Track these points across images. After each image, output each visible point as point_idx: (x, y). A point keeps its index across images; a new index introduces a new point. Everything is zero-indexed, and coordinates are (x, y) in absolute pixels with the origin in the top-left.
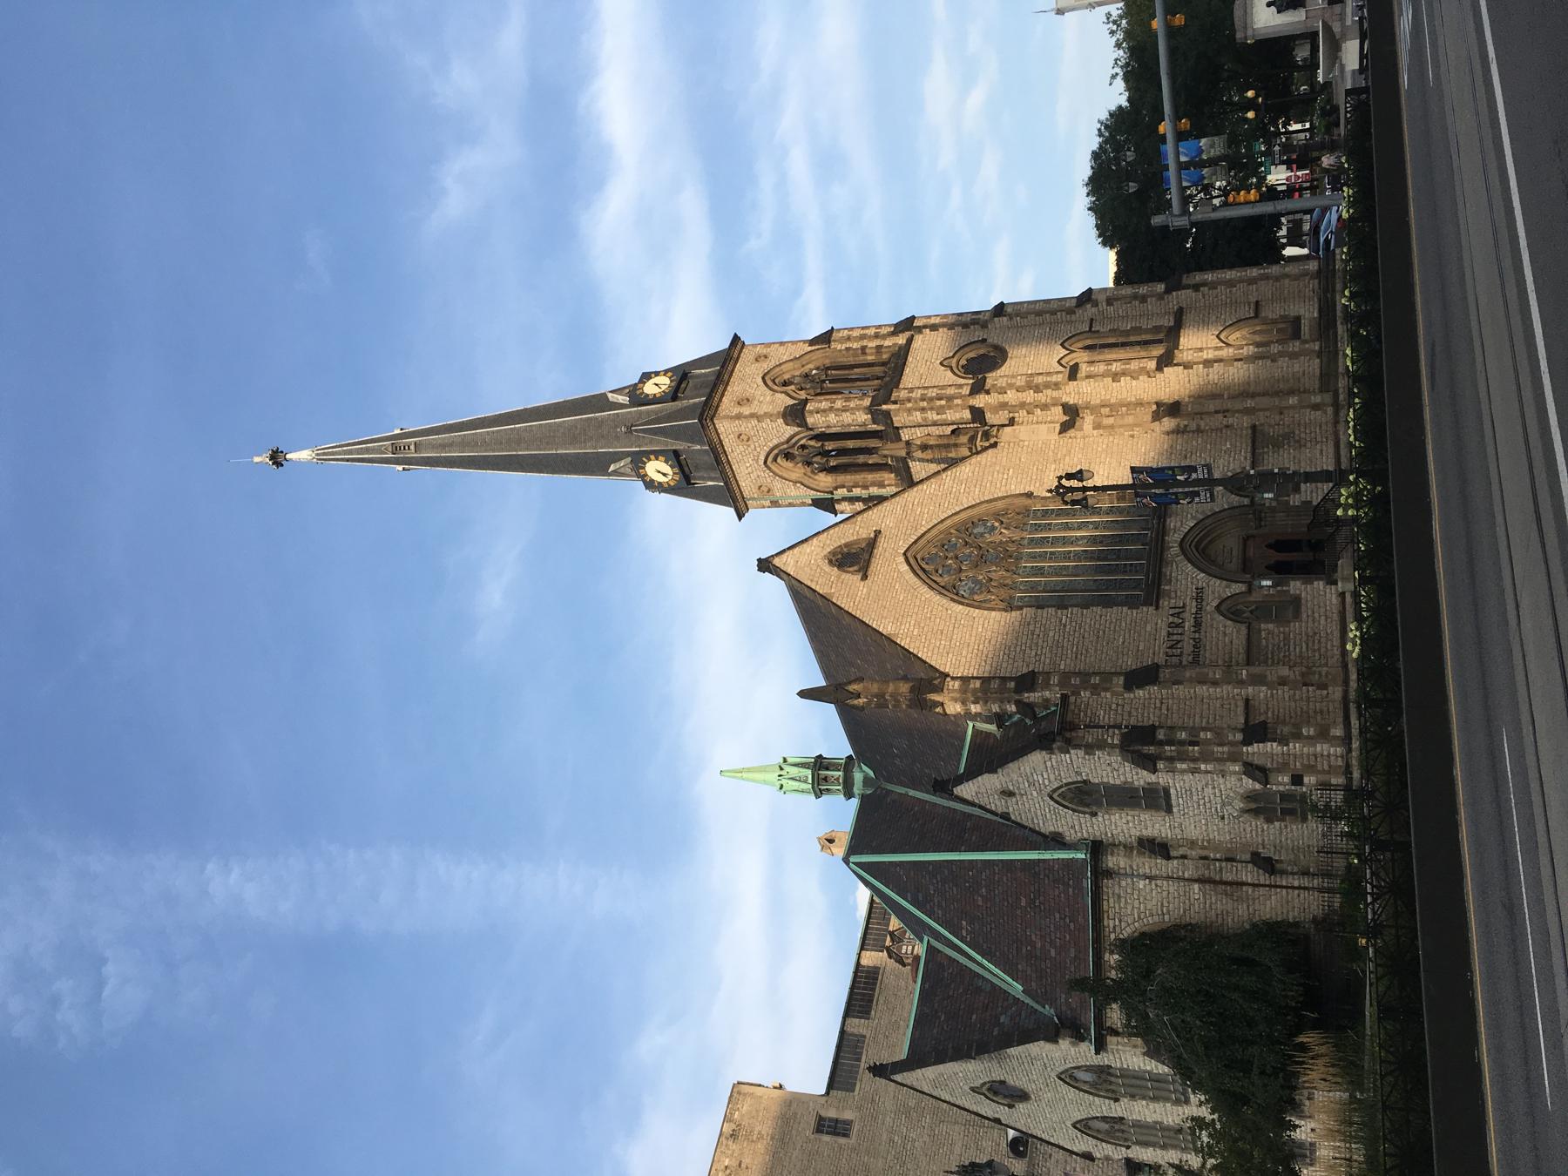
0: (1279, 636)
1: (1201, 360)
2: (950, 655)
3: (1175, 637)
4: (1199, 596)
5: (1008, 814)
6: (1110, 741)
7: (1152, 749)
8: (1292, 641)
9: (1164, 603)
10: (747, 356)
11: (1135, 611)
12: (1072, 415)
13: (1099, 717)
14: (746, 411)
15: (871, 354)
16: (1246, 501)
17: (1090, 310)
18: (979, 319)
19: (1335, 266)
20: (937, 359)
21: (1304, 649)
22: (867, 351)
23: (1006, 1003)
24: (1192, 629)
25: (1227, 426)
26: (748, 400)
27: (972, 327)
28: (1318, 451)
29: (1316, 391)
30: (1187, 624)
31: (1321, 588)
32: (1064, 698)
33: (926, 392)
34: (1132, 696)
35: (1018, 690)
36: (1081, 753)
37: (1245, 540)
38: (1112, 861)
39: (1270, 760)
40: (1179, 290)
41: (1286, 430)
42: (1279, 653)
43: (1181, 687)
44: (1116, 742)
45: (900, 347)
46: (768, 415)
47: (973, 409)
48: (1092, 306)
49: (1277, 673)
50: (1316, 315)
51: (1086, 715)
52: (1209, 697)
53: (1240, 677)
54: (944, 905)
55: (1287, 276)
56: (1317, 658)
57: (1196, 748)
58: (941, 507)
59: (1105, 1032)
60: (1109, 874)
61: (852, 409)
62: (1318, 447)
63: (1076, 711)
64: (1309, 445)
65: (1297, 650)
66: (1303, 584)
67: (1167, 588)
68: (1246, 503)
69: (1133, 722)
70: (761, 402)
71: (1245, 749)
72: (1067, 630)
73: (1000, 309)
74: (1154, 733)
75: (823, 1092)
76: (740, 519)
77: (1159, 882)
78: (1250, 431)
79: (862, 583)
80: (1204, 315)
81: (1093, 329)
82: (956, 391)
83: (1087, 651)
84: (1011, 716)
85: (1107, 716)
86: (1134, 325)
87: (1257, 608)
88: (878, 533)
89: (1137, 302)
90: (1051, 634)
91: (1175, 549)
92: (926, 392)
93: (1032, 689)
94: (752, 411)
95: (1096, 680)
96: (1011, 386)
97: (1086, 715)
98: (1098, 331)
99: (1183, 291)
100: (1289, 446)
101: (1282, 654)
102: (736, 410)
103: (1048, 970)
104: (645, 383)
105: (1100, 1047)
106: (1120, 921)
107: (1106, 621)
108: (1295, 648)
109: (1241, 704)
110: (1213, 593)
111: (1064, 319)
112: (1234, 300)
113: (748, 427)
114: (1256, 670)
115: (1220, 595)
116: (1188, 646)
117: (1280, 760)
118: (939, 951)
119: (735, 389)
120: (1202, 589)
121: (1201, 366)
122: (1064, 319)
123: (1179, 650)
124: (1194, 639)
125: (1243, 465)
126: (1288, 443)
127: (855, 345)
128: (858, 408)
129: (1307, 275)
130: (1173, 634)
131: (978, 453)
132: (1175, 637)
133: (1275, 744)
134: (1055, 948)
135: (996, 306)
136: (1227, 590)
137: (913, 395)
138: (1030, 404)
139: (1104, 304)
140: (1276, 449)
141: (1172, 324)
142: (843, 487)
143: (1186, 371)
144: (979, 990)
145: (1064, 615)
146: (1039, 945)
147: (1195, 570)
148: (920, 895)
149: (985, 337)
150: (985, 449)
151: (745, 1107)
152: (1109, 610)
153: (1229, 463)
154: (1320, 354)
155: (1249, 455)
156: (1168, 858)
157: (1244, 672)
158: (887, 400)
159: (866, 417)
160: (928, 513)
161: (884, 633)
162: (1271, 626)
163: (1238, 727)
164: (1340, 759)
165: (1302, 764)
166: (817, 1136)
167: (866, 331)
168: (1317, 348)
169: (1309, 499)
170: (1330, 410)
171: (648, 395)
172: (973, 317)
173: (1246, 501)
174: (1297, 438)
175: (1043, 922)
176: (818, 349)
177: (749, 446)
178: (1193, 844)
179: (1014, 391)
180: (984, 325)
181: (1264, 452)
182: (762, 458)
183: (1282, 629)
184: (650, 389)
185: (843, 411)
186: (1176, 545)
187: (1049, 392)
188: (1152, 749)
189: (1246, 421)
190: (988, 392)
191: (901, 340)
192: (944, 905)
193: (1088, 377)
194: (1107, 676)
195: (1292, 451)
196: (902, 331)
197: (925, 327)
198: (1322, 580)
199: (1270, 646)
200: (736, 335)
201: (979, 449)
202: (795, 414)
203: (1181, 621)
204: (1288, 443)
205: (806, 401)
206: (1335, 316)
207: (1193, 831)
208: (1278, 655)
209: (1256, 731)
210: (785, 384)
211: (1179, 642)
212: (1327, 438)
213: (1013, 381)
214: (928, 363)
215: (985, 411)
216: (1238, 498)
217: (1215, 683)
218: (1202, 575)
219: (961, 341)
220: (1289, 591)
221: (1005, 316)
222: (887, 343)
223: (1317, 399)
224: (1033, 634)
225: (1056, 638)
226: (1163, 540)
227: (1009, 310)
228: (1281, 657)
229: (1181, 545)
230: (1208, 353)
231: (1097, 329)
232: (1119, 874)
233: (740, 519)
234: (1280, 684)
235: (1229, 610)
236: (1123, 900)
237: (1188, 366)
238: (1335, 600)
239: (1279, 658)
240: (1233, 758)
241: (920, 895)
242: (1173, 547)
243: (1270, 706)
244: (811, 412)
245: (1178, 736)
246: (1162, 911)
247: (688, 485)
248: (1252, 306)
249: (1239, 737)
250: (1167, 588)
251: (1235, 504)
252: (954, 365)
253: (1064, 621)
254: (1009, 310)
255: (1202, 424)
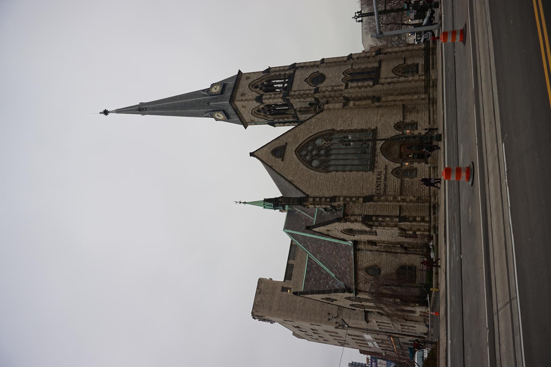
0: (410, 183)
1: (387, 82)
2: (309, 188)
3: (378, 183)
4: (386, 168)
5: (329, 234)
6: (358, 220)
7: (371, 223)
8: (414, 184)
9: (375, 170)
10: (244, 78)
11: (366, 173)
12: (347, 100)
13: (355, 211)
14: (244, 98)
15: (282, 76)
16: (401, 133)
17: (351, 61)
18: (316, 64)
19: (430, 47)
20: (303, 79)
21: (418, 187)
22: (281, 75)
23: (330, 279)
24: (384, 180)
25: (395, 105)
26: (244, 94)
27: (314, 67)
28: (423, 114)
29: (423, 93)
30: (382, 179)
31: (424, 165)
32: (345, 205)
33: (300, 92)
34: (365, 204)
35: (331, 201)
36: (350, 223)
37: (401, 146)
38: (361, 246)
39: (406, 227)
40: (380, 54)
41: (414, 106)
42: (410, 189)
43: (380, 202)
44: (360, 220)
45: (292, 74)
46: (250, 100)
47: (315, 98)
48: (352, 60)
49: (409, 198)
50: (423, 63)
51: (351, 211)
52: (389, 205)
53: (398, 199)
54: (312, 248)
55: (414, 50)
56: (422, 190)
57: (384, 223)
58: (306, 134)
59: (358, 291)
60: (359, 250)
61: (277, 98)
62: (424, 112)
63: (348, 209)
64: (420, 111)
65: (416, 188)
66: (418, 163)
67: (376, 165)
68: (401, 134)
69: (365, 213)
70: (249, 95)
71: (399, 223)
72: (345, 179)
73: (323, 60)
74: (373, 197)
75: (283, 280)
76: (246, 129)
77: (373, 252)
78: (402, 106)
79: (282, 162)
80: (388, 63)
81: (353, 68)
82: (309, 92)
83: (351, 188)
84: (328, 208)
85: (357, 211)
86: (365, 66)
87: (404, 172)
88: (286, 143)
89: (367, 59)
90: (341, 181)
91: (379, 150)
92: (300, 92)
93: (335, 202)
94: (246, 98)
95: (354, 199)
96: (327, 90)
97: (351, 211)
98: (354, 68)
99: (381, 55)
100: (415, 112)
101: (411, 189)
102: (241, 98)
103: (342, 272)
104: (212, 88)
105: (356, 294)
106: (362, 262)
107: (357, 176)
108: (415, 187)
109: (398, 207)
110: (390, 167)
111: (343, 64)
112: (397, 57)
113: (245, 103)
114: (403, 197)
115: (392, 168)
116: (382, 186)
117: (410, 227)
118: (311, 259)
119: (240, 90)
120: (387, 165)
121: (387, 84)
122: (343, 64)
123: (380, 188)
124: (384, 183)
125: (400, 119)
126: (414, 111)
127: (277, 73)
128: (279, 98)
129: (421, 49)
130: (378, 182)
131: (317, 114)
132: (378, 183)
133: (408, 223)
134: (344, 267)
135: (321, 59)
136: (395, 166)
137: (296, 93)
138: (333, 96)
139: (356, 59)
140: (410, 113)
141: (378, 66)
142: (276, 119)
143: (382, 86)
144: (322, 273)
145: (344, 174)
146: (339, 265)
147: (385, 158)
148: (305, 245)
149: (318, 70)
150: (319, 112)
151: (262, 285)
152: (358, 173)
153: (396, 118)
154: (424, 80)
155: (402, 116)
156: (376, 246)
157: (399, 198)
158: (288, 95)
159: (281, 100)
160: (302, 136)
161: (289, 180)
162: (408, 179)
163: (397, 215)
164: (427, 226)
165: (416, 229)
166: (282, 292)
167: (280, 68)
168: (424, 78)
169: (420, 132)
170: (427, 100)
171: (213, 93)
172: (314, 63)
173: (401, 133)
174: (417, 109)
175: (340, 260)
176: (266, 75)
177: (246, 109)
178: (383, 242)
179: (328, 92)
180: (318, 66)
181: (406, 114)
182: (250, 111)
183: (411, 180)
184: (213, 90)
185: (274, 99)
186: (379, 149)
187: (339, 92)
188: (371, 223)
189: (401, 103)
190: (319, 93)
191: (292, 72)
192: (312, 248)
193: (351, 88)
194: (358, 198)
195: (415, 114)
196: (292, 68)
197: (299, 67)
198: (424, 162)
199: (407, 187)
200: (239, 70)
201: (318, 112)
202: (259, 99)
203: (380, 177)
204: (414, 111)
205: (262, 95)
206: (430, 64)
207: (383, 239)
208: (410, 189)
209: (403, 219)
210: (257, 87)
211: (380, 184)
212: (426, 109)
213: (327, 89)
214: (300, 80)
215: (319, 99)
216: (398, 131)
217: (390, 202)
218: (387, 160)
219: (311, 72)
220: (413, 166)
221: (324, 63)
222: (287, 72)
223: (423, 96)
224: (335, 181)
225: (342, 183)
226: (375, 147)
227: (326, 61)
228: (411, 191)
229: (381, 148)
230: (389, 80)
231: (354, 67)
232: (362, 250)
233: (246, 129)
234: (410, 202)
235: (396, 172)
236: (363, 257)
237: (383, 84)
238: (427, 169)
239: (410, 191)
240: (396, 226)
241: (305, 245)
242: (378, 150)
243: (407, 208)
244: (264, 99)
245: (379, 219)
246: (374, 260)
247: (228, 119)
248: (403, 59)
249: (397, 220)
250: (376, 165)
251: (398, 134)
252: (309, 81)
253: (344, 177)
254: (326, 61)
255: (387, 104)
